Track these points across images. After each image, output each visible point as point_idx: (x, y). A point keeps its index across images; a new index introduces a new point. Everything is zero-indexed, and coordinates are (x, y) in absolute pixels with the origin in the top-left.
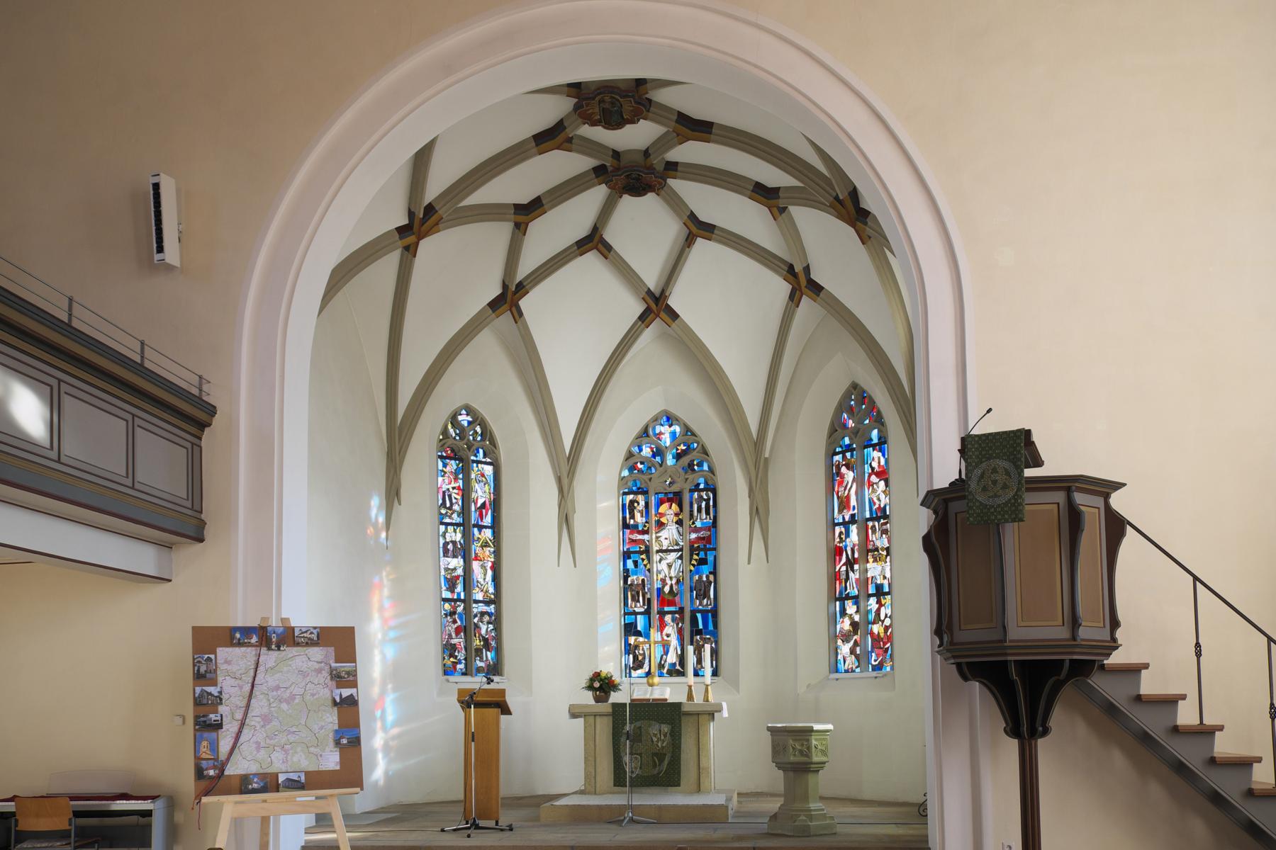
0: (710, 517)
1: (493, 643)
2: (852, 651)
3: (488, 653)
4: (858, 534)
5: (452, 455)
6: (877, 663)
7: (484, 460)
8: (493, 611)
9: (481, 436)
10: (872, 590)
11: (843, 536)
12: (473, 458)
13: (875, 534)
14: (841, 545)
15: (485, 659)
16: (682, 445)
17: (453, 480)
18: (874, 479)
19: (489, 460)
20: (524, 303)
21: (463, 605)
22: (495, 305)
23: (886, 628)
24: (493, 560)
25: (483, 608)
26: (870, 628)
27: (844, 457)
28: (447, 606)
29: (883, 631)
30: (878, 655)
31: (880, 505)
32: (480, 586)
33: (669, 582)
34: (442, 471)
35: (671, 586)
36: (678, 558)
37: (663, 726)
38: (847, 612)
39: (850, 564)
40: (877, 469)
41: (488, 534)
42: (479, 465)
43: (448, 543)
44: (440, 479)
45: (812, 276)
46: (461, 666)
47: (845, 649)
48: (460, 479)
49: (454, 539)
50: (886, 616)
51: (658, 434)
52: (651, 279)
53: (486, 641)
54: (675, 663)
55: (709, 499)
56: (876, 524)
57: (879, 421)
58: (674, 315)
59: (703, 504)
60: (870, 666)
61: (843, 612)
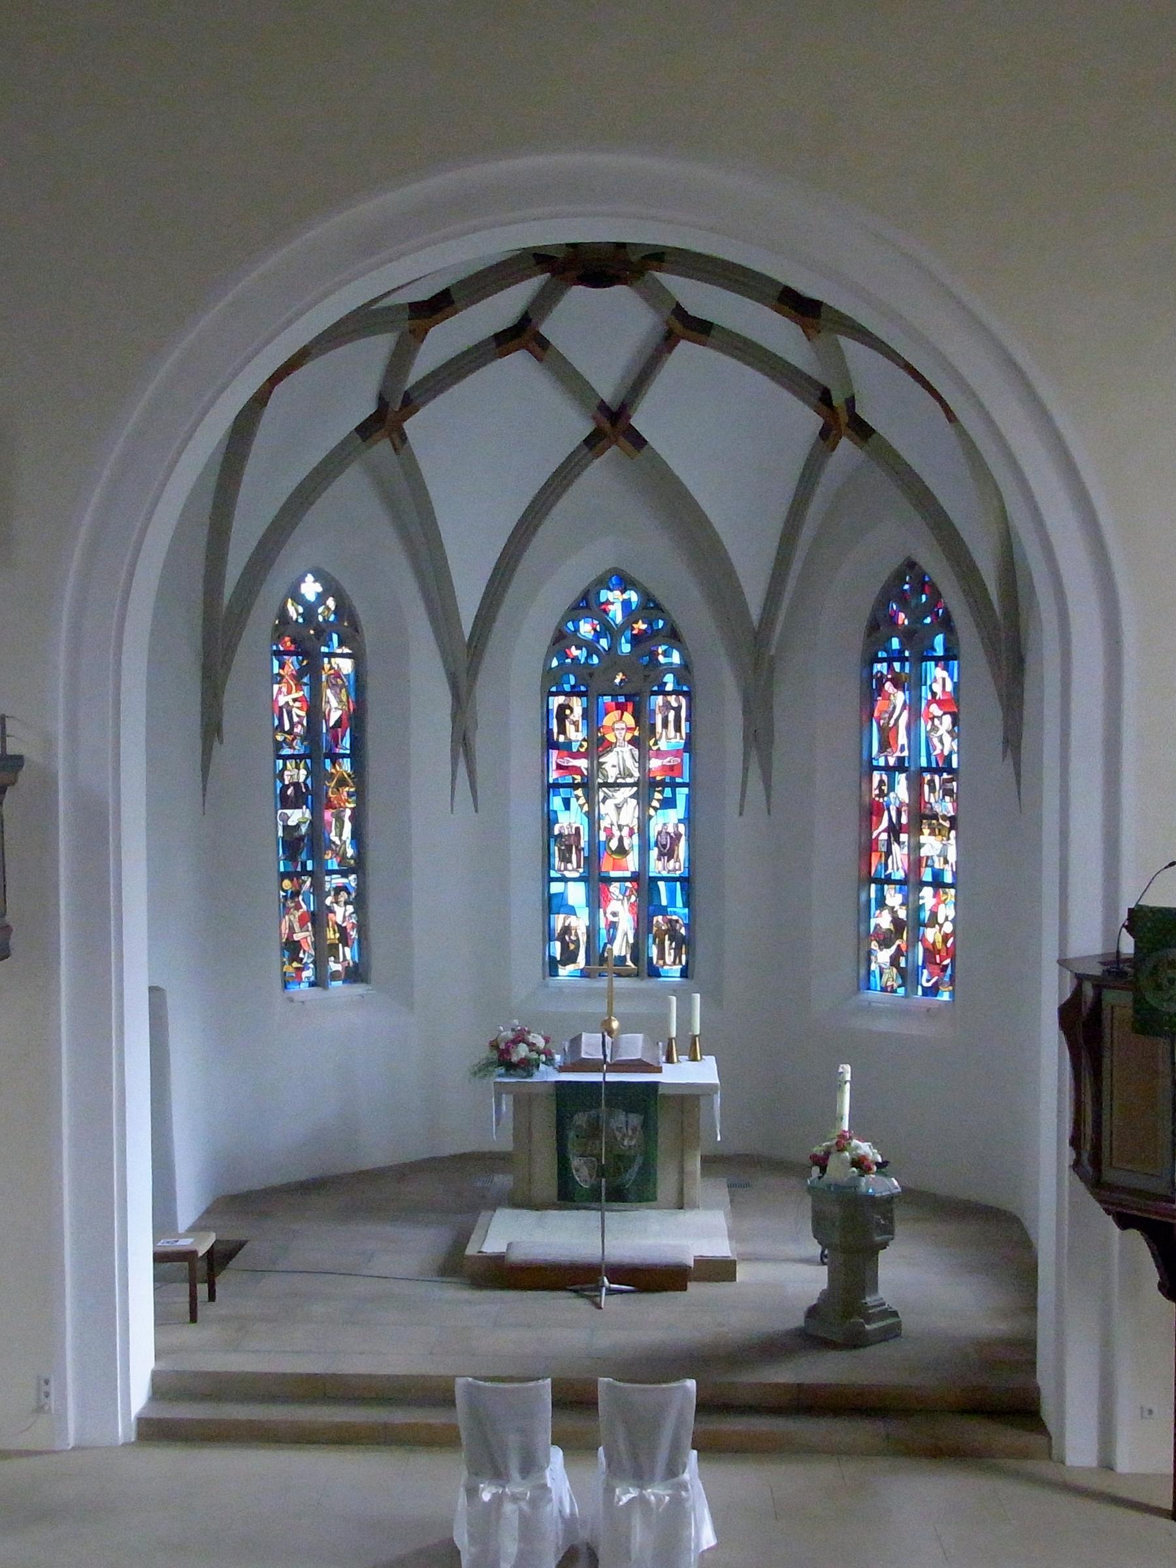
0: (681, 736)
1: (354, 934)
2: (894, 961)
3: (347, 950)
4: (909, 788)
5: (292, 648)
6: (929, 984)
7: (339, 651)
8: (353, 884)
9: (335, 614)
10: (927, 876)
11: (885, 788)
12: (324, 649)
13: (934, 793)
14: (881, 800)
15: (341, 960)
16: (640, 622)
17: (294, 687)
18: (935, 710)
19: (346, 650)
20: (408, 426)
21: (310, 879)
22: (366, 430)
23: (946, 938)
24: (352, 805)
25: (338, 880)
26: (921, 933)
27: (890, 667)
28: (287, 884)
29: (940, 940)
30: (931, 975)
31: (942, 750)
32: (334, 847)
33: (617, 833)
34: (279, 674)
35: (621, 839)
36: (632, 797)
37: (631, 1116)
38: (887, 902)
39: (894, 830)
40: (939, 695)
41: (346, 765)
42: (333, 660)
43: (287, 787)
44: (276, 687)
45: (858, 411)
46: (308, 974)
47: (883, 956)
48: (306, 684)
49: (295, 780)
50: (946, 919)
51: (603, 603)
52: (607, 389)
53: (342, 930)
54: (625, 957)
55: (680, 707)
56: (937, 778)
57: (946, 624)
58: (638, 441)
59: (672, 715)
60: (920, 988)
61: (881, 903)
